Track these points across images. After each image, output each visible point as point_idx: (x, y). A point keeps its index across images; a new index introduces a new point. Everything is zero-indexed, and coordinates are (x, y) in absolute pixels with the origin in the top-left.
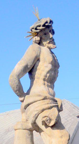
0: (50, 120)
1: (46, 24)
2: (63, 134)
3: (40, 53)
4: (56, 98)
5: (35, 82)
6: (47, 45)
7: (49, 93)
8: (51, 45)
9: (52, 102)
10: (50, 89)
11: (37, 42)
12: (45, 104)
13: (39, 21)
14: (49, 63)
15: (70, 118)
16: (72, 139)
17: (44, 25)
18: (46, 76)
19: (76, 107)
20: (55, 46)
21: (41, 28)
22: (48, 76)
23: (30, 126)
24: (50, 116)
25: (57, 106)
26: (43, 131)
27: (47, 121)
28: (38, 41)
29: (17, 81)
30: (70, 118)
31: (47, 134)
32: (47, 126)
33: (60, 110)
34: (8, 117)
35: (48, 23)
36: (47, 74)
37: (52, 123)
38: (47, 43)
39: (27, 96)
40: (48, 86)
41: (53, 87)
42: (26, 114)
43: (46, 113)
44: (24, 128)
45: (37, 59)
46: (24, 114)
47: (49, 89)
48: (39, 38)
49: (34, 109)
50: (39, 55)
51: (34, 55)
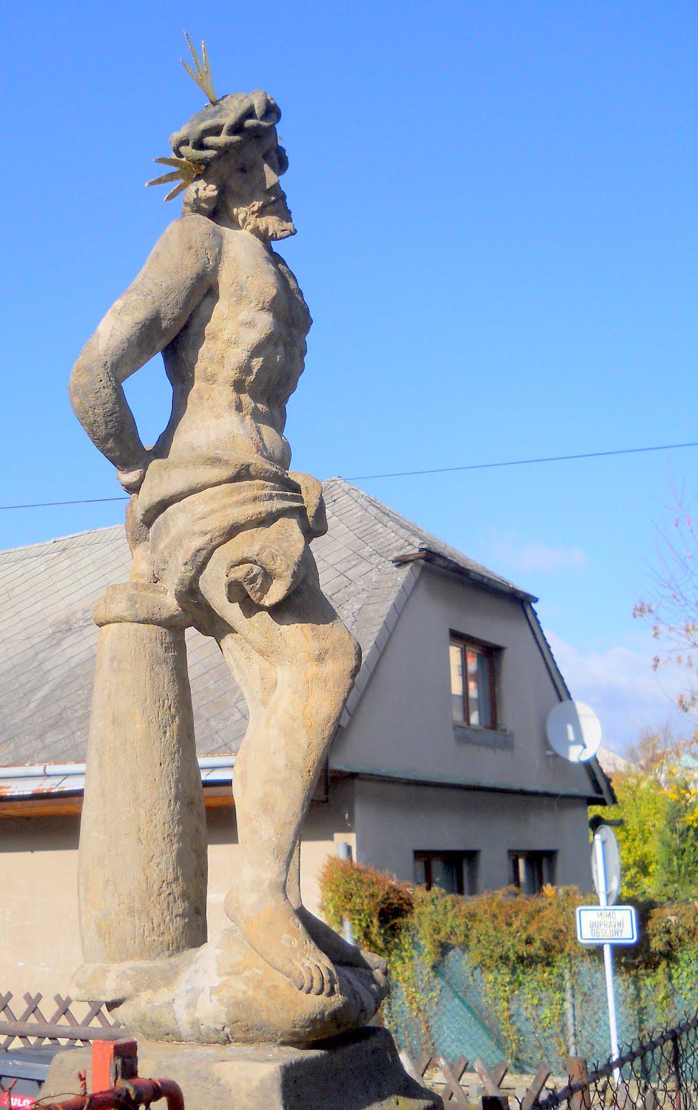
0: (268, 577)
1: (249, 123)
2: (326, 644)
3: (218, 259)
4: (294, 474)
5: (192, 395)
6: (252, 219)
7: (262, 449)
8: (271, 223)
10: (267, 431)
12: (244, 502)
13: (213, 109)
14: (261, 305)
17: (237, 129)
18: (246, 369)
20: (289, 226)
21: (223, 139)
22: (255, 371)
23: (170, 604)
24: (264, 557)
25: (300, 513)
27: (253, 581)
28: (208, 200)
30: (364, 567)
32: (250, 607)
33: (314, 527)
34: (66, 563)
36: (251, 357)
37: (277, 592)
39: (155, 464)
40: (256, 416)
41: (277, 420)
43: (247, 544)
44: (143, 615)
46: (141, 551)
48: (213, 187)
50: (215, 270)
51: (190, 268)
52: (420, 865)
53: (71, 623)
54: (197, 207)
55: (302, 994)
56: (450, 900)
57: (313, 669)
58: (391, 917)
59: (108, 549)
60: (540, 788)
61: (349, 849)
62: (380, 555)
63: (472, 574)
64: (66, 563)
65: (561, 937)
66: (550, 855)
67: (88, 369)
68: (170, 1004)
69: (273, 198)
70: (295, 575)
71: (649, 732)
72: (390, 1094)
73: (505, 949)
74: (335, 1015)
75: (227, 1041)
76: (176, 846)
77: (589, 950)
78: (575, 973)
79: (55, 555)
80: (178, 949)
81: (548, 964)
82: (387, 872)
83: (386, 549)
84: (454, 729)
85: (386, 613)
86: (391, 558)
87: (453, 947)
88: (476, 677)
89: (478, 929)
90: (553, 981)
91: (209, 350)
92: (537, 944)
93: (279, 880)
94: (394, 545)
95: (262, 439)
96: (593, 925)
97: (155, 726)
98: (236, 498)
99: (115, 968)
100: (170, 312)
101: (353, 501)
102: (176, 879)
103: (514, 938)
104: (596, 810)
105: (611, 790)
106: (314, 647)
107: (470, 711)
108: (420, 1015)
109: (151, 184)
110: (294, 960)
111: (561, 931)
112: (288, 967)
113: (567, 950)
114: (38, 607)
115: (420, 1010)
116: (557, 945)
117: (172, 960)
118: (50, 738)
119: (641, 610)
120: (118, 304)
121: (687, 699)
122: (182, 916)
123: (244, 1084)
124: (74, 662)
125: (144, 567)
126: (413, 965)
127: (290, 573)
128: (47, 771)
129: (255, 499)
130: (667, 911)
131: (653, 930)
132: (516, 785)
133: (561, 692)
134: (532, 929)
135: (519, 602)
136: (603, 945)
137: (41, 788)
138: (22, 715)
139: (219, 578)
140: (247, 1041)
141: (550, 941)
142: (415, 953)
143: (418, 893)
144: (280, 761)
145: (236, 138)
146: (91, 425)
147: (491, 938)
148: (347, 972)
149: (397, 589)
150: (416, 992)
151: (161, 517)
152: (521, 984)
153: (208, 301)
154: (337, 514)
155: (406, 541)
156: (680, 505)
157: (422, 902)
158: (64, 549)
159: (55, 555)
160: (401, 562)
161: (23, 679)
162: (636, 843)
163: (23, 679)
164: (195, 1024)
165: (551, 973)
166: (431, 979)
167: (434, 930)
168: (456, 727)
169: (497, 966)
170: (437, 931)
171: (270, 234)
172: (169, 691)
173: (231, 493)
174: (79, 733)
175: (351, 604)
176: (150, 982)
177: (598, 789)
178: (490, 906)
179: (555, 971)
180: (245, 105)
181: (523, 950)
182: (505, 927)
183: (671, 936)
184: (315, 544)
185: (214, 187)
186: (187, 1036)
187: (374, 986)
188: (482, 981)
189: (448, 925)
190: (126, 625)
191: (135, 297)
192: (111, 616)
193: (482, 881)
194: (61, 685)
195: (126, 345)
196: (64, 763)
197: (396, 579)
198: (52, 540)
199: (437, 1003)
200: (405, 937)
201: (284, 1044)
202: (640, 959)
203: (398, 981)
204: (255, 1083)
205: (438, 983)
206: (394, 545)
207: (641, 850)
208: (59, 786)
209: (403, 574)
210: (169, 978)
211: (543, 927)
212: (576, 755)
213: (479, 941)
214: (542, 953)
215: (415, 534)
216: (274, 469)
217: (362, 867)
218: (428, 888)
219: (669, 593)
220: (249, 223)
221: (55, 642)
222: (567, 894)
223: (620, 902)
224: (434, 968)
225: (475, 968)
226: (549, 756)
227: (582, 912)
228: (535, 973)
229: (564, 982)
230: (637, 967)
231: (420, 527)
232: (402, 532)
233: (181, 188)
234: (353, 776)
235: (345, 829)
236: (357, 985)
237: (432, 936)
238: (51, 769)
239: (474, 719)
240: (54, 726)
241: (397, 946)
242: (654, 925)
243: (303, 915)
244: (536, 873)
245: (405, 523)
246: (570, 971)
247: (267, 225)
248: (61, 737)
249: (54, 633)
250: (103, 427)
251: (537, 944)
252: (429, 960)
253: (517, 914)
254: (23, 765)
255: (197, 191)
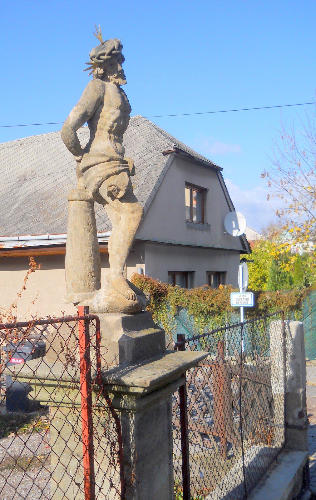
0: (119, 190)
1: (114, 52)
2: (135, 208)
3: (104, 94)
4: (126, 158)
5: (96, 134)
6: (114, 79)
7: (116, 151)
8: (119, 81)
9: (120, 164)
10: (118, 145)
11: (100, 76)
12: (112, 168)
13: (103, 46)
14: (116, 108)
15: (149, 156)
16: (152, 199)
17: (110, 54)
18: (112, 127)
19: (161, 133)
20: (125, 81)
21: (105, 57)
22: (115, 127)
23: (90, 195)
24: (118, 185)
25: (127, 170)
26: (108, 203)
27: (115, 191)
28: (101, 74)
29: (72, 135)
30: (150, 155)
31: (113, 207)
32: (113, 198)
33: (131, 173)
34: (23, 150)
35: (116, 50)
36: (113, 123)
37: (121, 194)
38: (114, 78)
39: (85, 155)
40: (115, 140)
41: (120, 141)
42: (85, 179)
43: (113, 180)
44: (82, 199)
45: (100, 103)
46: (81, 179)
47: (116, 145)
48: (102, 70)
49: (96, 173)
50: (103, 97)
51: (96, 97)
52: (171, 277)
53: (26, 177)
54: (97, 76)
55: (127, 300)
56: (182, 290)
57: (131, 215)
58: (158, 296)
59: (41, 145)
60: (220, 247)
61: (142, 270)
62: (157, 150)
63: (195, 158)
64: (23, 150)
65: (225, 304)
66: (224, 273)
67: (67, 128)
68: (92, 303)
69: (120, 74)
70: (126, 190)
71: (272, 223)
72: (150, 327)
73: (203, 309)
74: (136, 305)
75: (107, 312)
76: (92, 263)
77: (235, 309)
78: (229, 317)
79: (18, 147)
80: (94, 290)
81: (219, 314)
82: (157, 280)
83: (160, 148)
84: (186, 223)
85: (159, 175)
86: (162, 151)
87: (183, 308)
88: (196, 199)
89: (193, 301)
90: (221, 321)
91: (101, 121)
92: (215, 307)
93: (121, 271)
94: (163, 146)
95: (116, 147)
96: (237, 299)
97: (86, 230)
98: (109, 166)
99: (77, 295)
100: (90, 110)
101: (146, 126)
102: (93, 272)
103: (206, 304)
104: (242, 256)
105: (250, 247)
106: (131, 209)
107: (193, 215)
108: (169, 334)
109: (84, 71)
110: (125, 292)
111: (225, 302)
112: (123, 294)
113: (226, 309)
114: (12, 169)
115: (169, 332)
116: (223, 307)
117: (92, 292)
118: (20, 225)
119: (263, 175)
120: (75, 108)
121: (280, 212)
122: (95, 281)
123: (112, 322)
124: (28, 194)
125: (82, 184)
126: (166, 315)
127: (125, 189)
128: (19, 239)
129: (115, 167)
130: (266, 294)
131: (260, 301)
132: (211, 246)
133: (231, 208)
134: (213, 301)
135: (215, 170)
136: (240, 307)
137: (17, 245)
138: (9, 215)
139: (105, 189)
140: (112, 312)
141: (220, 305)
142: (167, 310)
143: (170, 287)
144: (122, 240)
145: (110, 57)
146: (67, 144)
147: (197, 305)
148: (140, 297)
149: (164, 165)
150: (167, 325)
151: (88, 170)
152: (208, 322)
153: (101, 106)
154: (140, 131)
155: (168, 144)
156: (284, 130)
157: (171, 291)
158: (22, 144)
159: (18, 147)
160: (166, 153)
161: (7, 200)
162: (262, 269)
163: (7, 200)
164: (99, 308)
165: (220, 318)
166: (174, 320)
167: (175, 301)
168: (187, 222)
169: (199, 315)
170: (176, 302)
171: (119, 84)
172: (90, 220)
173: (108, 165)
174: (32, 223)
175: (144, 171)
176: (86, 298)
177: (245, 248)
178: (197, 293)
179: (222, 317)
180: (112, 47)
181: (209, 309)
182: (203, 300)
183: (267, 304)
184: (132, 178)
185: (103, 70)
186: (97, 311)
187: (146, 300)
188: (193, 321)
189: (181, 300)
190: (78, 201)
191: (80, 106)
192: (73, 199)
193: (196, 282)
194: (23, 203)
195: (78, 121)
196: (26, 235)
197: (163, 161)
198: (16, 140)
199: (176, 329)
200: (164, 304)
201: (122, 313)
202: (254, 312)
203: (161, 321)
204: (115, 321)
205: (176, 322)
206: (163, 146)
207: (263, 272)
208: (25, 245)
209: (166, 159)
210: (92, 297)
211: (218, 301)
212: (235, 233)
213: (193, 306)
214: (217, 310)
215: (172, 141)
216: (120, 158)
217: (147, 277)
218: (174, 286)
219: (277, 167)
220: (113, 81)
221: (19, 185)
222: (228, 288)
223: (248, 291)
224: (175, 316)
225: (191, 316)
226: (225, 234)
227: (251, 304)
228: (214, 318)
229: (225, 321)
230: (253, 316)
231: (174, 137)
232: (167, 140)
233: (93, 71)
234: (145, 241)
235: (142, 263)
236: (141, 299)
237: (174, 304)
238: (21, 238)
239: (195, 219)
240: (21, 220)
241: (160, 308)
242: (261, 300)
243: (127, 280)
244: (218, 280)
245: (168, 135)
246: (228, 317)
247: (118, 81)
248: (25, 225)
249: (19, 181)
250: (71, 145)
251: (215, 307)
252: (173, 313)
253: (208, 295)
254: (9, 236)
255: (97, 71)
